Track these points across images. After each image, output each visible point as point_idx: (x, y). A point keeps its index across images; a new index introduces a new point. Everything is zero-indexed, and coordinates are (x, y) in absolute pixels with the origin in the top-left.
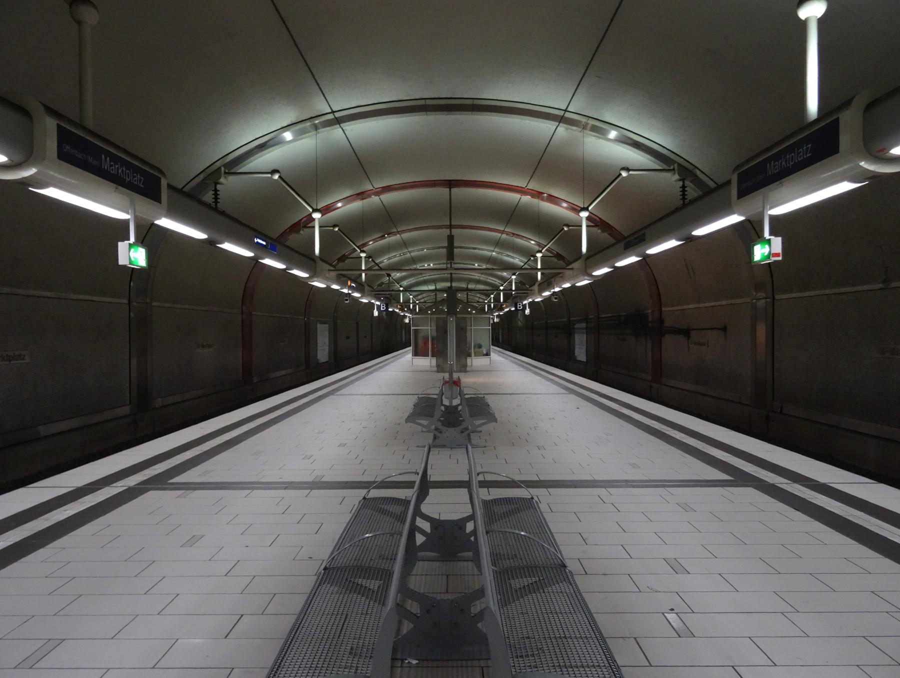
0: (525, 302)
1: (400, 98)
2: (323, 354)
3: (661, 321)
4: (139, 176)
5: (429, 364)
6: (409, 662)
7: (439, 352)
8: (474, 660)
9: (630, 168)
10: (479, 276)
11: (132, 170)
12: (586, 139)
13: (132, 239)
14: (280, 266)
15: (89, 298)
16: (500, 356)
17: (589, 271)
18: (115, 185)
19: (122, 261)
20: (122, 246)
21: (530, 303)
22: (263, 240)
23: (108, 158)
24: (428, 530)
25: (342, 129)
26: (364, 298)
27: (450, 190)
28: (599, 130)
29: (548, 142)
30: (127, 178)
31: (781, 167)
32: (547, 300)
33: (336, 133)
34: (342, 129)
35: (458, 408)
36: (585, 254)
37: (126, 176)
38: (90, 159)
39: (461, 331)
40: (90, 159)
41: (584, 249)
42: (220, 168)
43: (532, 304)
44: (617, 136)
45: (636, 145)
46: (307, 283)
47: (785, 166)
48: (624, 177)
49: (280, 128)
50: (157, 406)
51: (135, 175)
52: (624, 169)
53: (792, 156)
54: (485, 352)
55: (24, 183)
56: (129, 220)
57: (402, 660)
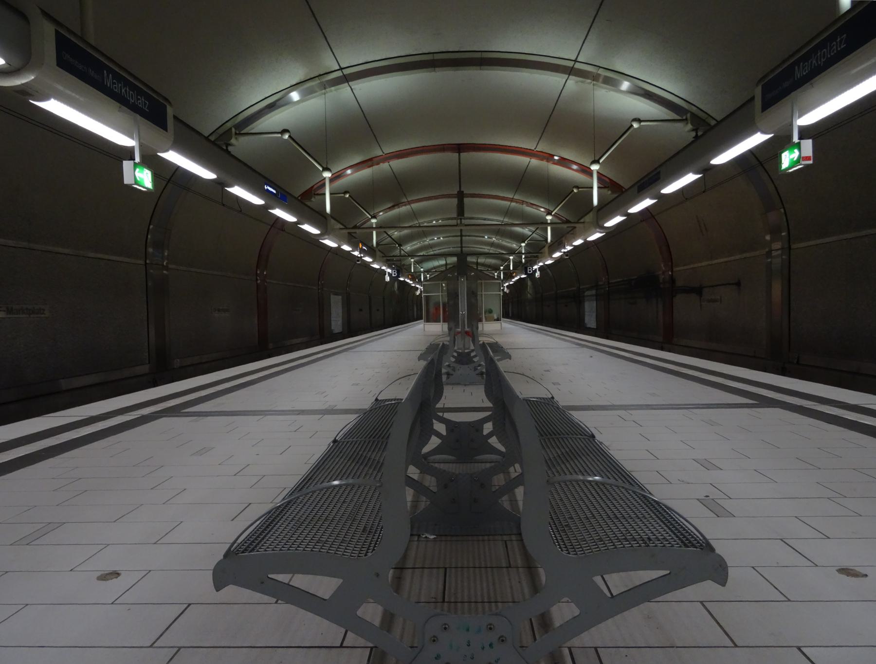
0: (535, 267)
1: (407, 53)
2: (337, 323)
3: (673, 280)
4: (143, 99)
5: (441, 330)
6: (426, 537)
7: (450, 315)
8: (495, 535)
9: (641, 119)
10: (488, 249)
11: (135, 92)
12: (596, 92)
13: (137, 160)
14: (290, 218)
15: (107, 257)
16: (510, 324)
17: (600, 223)
18: (118, 105)
19: (127, 180)
20: (127, 165)
22: (274, 189)
23: (111, 75)
24: (444, 433)
25: (351, 87)
26: (375, 263)
27: (459, 155)
28: (611, 83)
30: (131, 100)
31: (811, 66)
32: (558, 261)
33: (344, 92)
34: (351, 87)
35: (470, 355)
36: (596, 206)
37: (129, 97)
38: (92, 73)
39: (473, 295)
40: (92, 73)
41: (595, 201)
42: (231, 129)
43: (541, 269)
44: (629, 87)
45: (649, 95)
46: (318, 240)
47: (816, 65)
48: (635, 129)
49: (289, 86)
50: (175, 367)
51: (139, 97)
52: (635, 120)
53: (824, 52)
54: (496, 318)
55: (24, 92)
56: (133, 148)
57: (419, 536)
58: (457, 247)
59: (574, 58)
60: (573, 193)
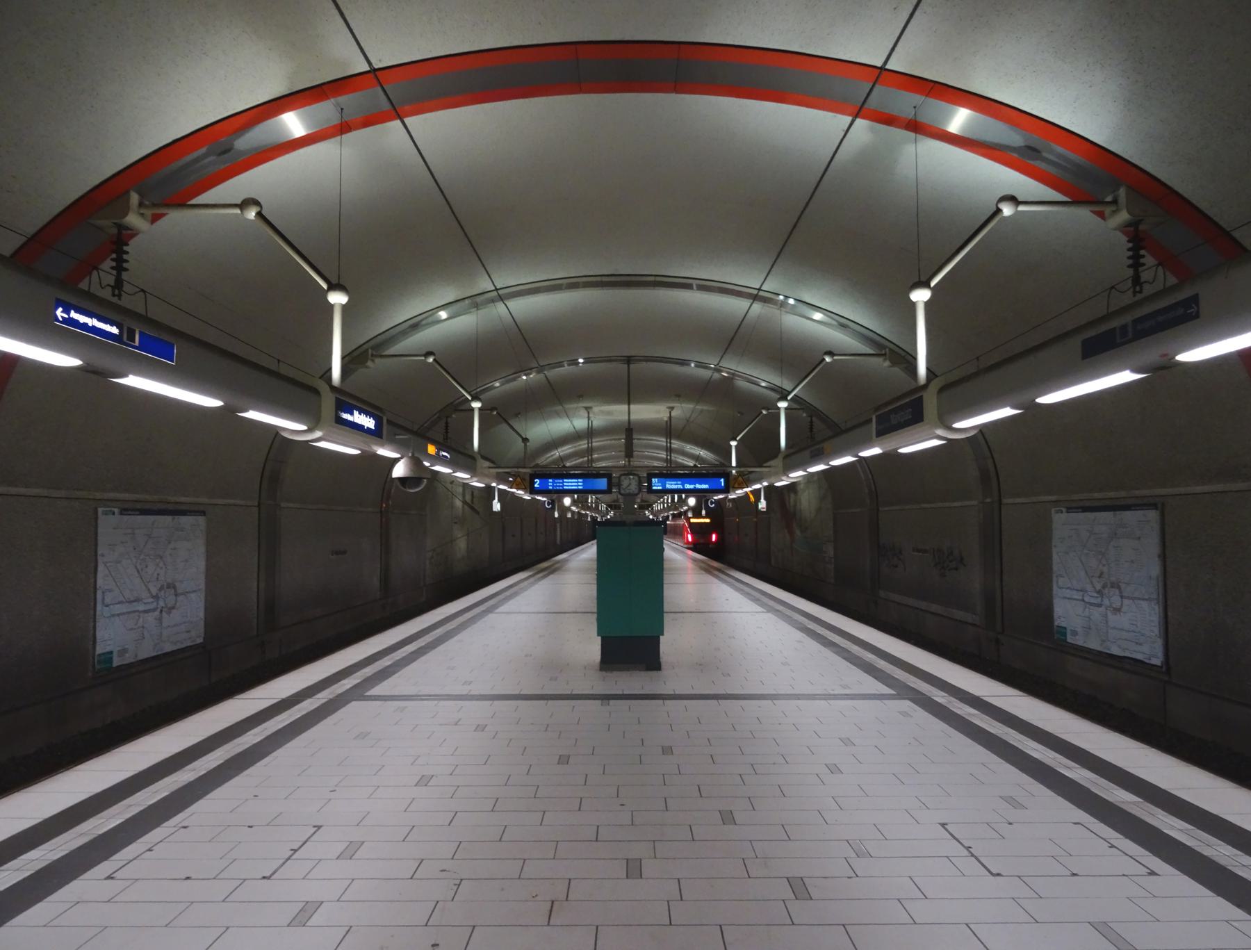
21: (765, 488)
29: (828, 160)
42: (367, 350)
58: (620, 451)
59: (758, 287)
60: (824, 363)
